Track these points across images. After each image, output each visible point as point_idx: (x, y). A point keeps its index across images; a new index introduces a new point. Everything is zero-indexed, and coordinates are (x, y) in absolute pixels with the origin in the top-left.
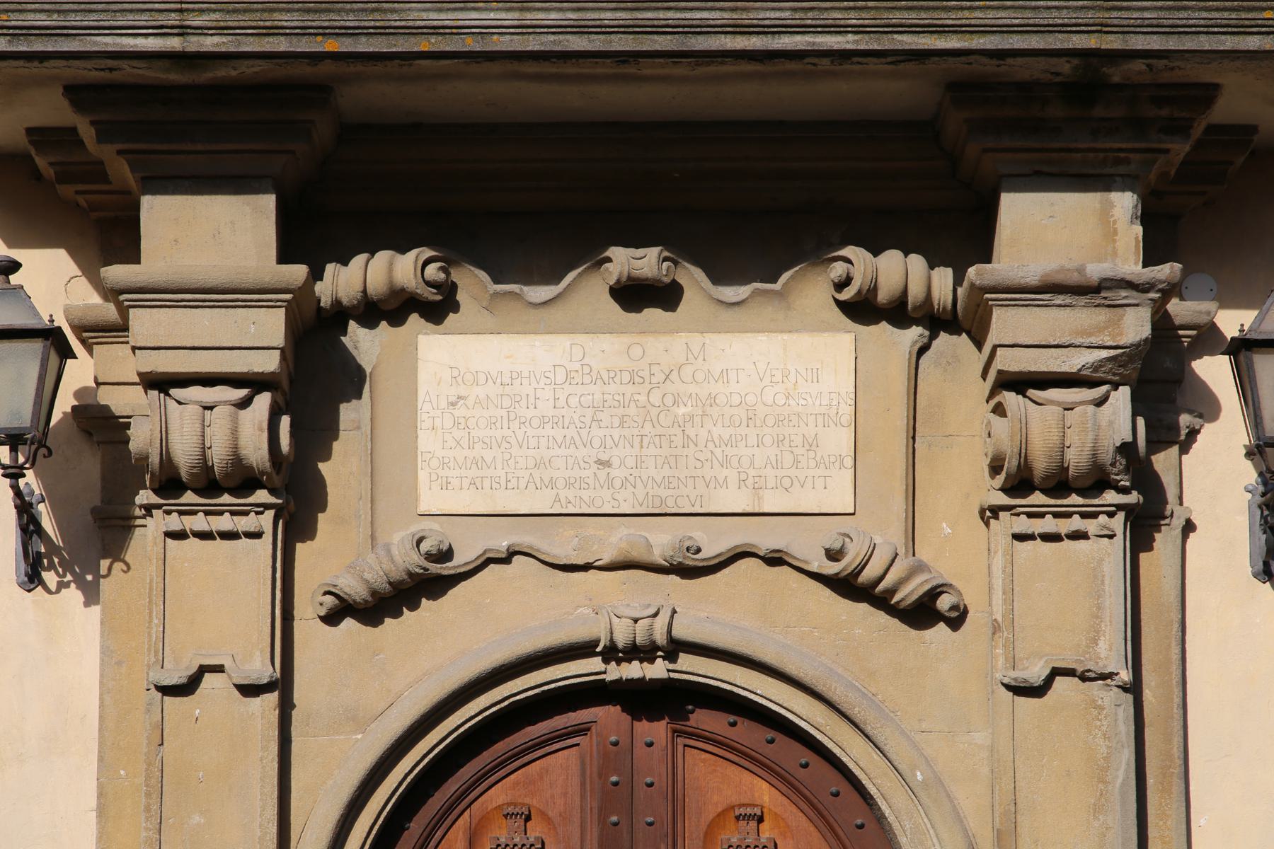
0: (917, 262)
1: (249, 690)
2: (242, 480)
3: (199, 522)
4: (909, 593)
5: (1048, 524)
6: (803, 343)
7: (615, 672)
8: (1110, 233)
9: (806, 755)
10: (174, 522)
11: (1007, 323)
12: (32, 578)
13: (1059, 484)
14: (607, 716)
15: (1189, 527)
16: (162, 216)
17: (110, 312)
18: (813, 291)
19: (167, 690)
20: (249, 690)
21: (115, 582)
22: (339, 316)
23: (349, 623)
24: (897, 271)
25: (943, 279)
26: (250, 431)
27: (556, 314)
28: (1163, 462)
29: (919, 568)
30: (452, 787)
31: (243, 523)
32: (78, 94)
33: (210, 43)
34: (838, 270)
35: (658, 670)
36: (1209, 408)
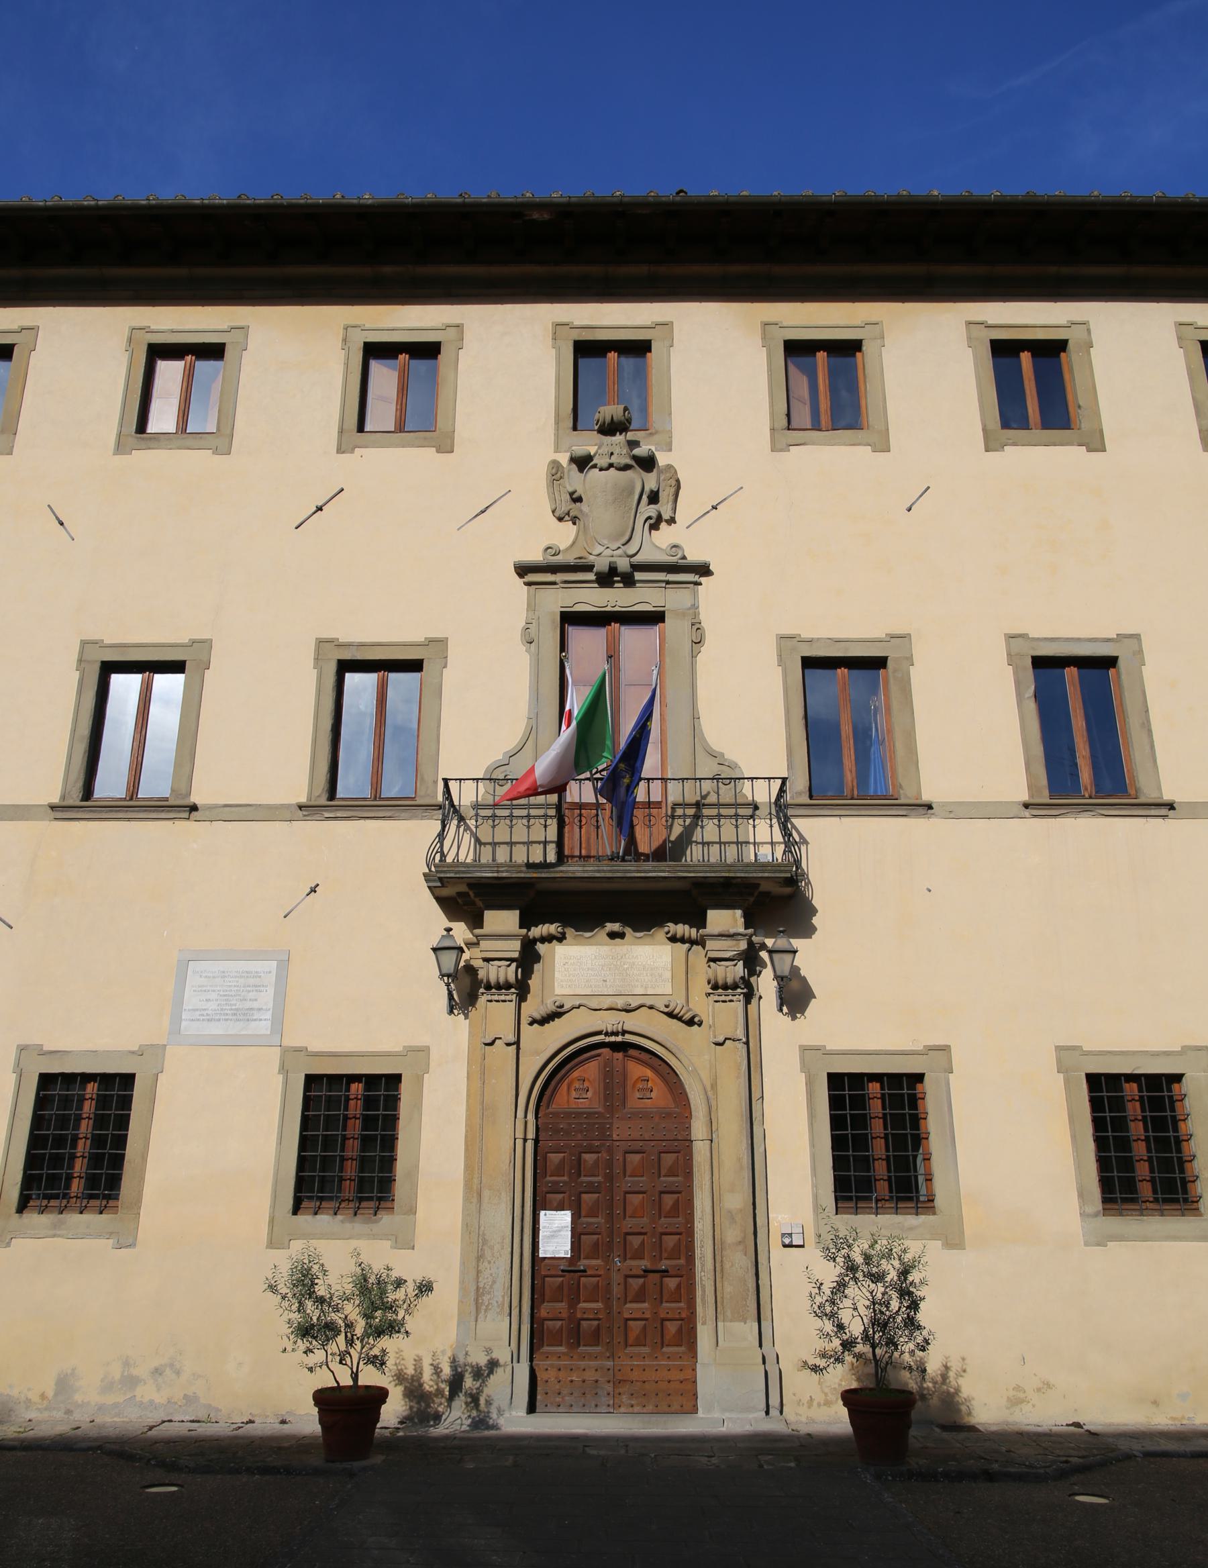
0: (687, 927)
1: (508, 1045)
2: (508, 986)
3: (496, 997)
4: (687, 1017)
5: (723, 998)
6: (658, 948)
7: (608, 1039)
8: (736, 921)
9: (660, 1063)
10: (489, 997)
11: (710, 944)
12: (451, 1012)
13: (726, 987)
14: (605, 1051)
15: (760, 997)
16: (489, 915)
17: (475, 940)
18: (660, 934)
19: (717, 1044)
20: (508, 1045)
21: (473, 1013)
22: (535, 941)
23: (535, 1025)
24: (681, 929)
25: (694, 931)
26: (510, 973)
27: (592, 940)
28: (753, 980)
29: (690, 1010)
30: (563, 1072)
31: (508, 998)
32: (469, 885)
33: (504, 875)
34: (666, 929)
35: (619, 1039)
36: (764, 965)
